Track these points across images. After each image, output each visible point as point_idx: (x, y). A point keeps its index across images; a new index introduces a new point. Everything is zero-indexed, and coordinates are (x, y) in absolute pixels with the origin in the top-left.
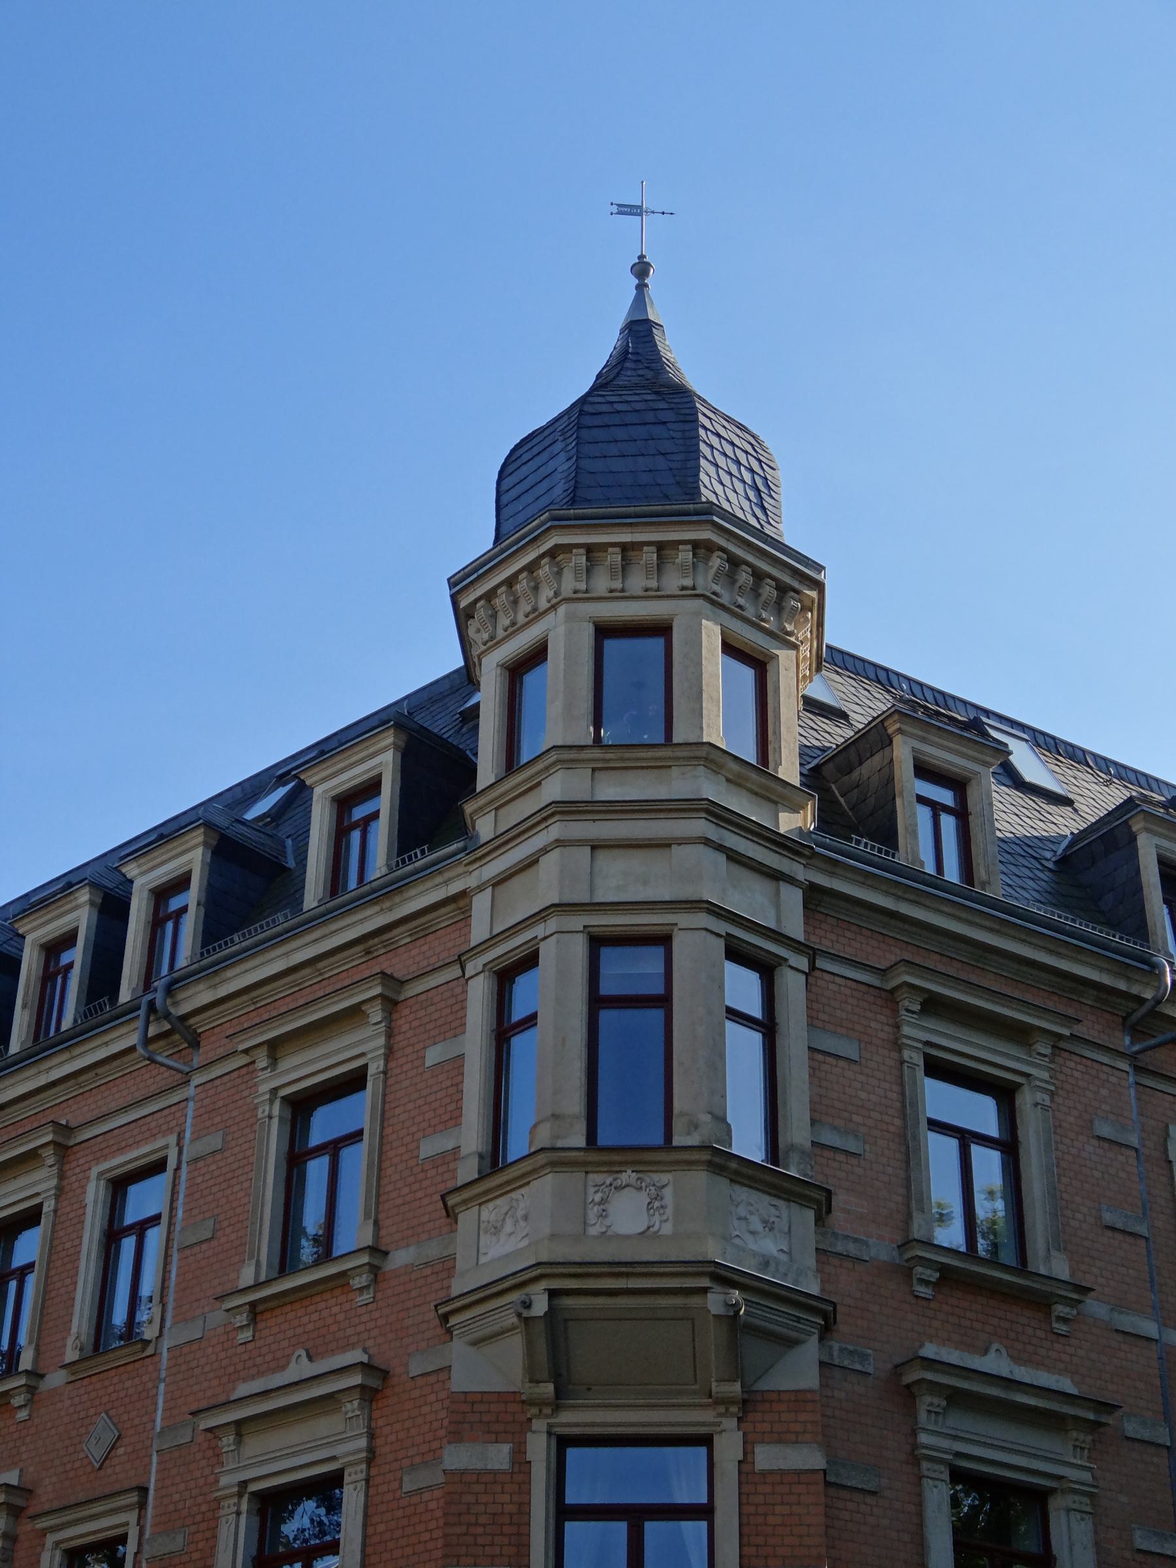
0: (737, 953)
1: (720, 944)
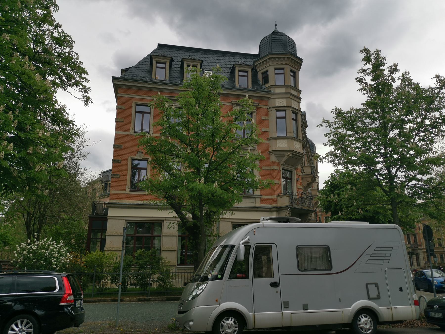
0: (293, 112)
1: (291, 111)
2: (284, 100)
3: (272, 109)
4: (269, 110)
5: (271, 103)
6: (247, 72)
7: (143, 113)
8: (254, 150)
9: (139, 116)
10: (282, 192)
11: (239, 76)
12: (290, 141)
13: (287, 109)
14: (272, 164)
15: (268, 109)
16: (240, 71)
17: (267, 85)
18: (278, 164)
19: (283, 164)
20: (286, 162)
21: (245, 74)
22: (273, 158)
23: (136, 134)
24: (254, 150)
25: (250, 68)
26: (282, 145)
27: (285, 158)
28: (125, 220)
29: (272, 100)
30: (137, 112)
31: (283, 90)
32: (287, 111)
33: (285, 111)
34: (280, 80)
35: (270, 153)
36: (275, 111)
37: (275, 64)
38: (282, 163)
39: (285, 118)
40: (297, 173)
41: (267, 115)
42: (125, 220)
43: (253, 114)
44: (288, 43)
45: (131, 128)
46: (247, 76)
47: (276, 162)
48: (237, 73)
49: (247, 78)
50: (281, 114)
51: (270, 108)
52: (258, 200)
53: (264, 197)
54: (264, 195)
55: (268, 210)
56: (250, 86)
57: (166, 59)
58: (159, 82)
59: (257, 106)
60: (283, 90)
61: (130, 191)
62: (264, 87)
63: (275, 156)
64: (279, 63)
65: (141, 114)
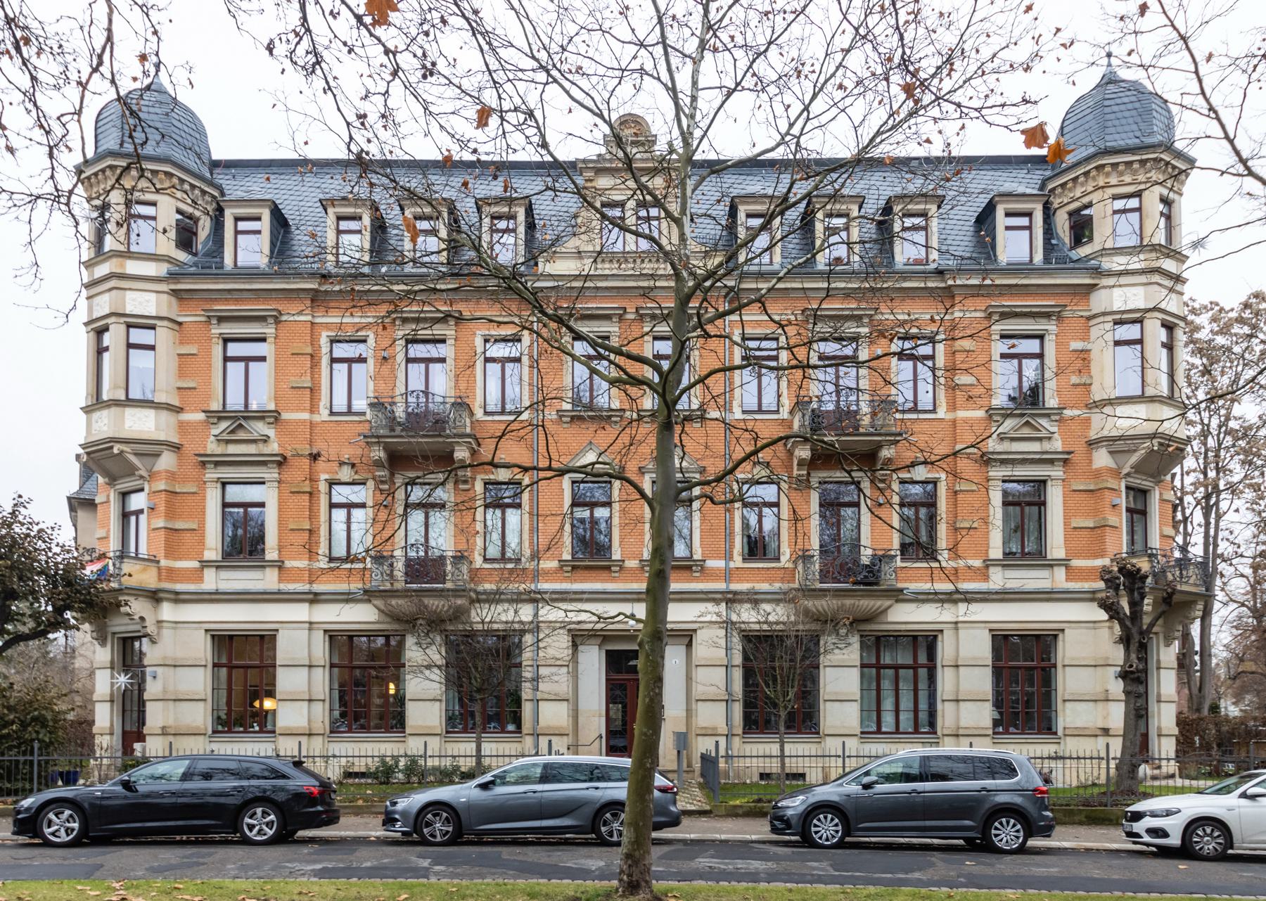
1: (1159, 323)
2: (1140, 291)
3: (1101, 319)
4: (1092, 322)
5: (1099, 301)
6: (1029, 214)
7: (247, 360)
8: (1050, 438)
9: (494, 369)
10: (1125, 550)
11: (1008, 228)
12: (114, 410)
13: (109, 321)
14: (1097, 474)
15: (1089, 318)
16: (1008, 215)
17: (1084, 251)
18: (1116, 473)
19: (1128, 475)
20: (1138, 469)
21: (1024, 221)
22: (1102, 459)
23: (490, 418)
24: (1050, 438)
25: (520, 205)
26: (1130, 420)
27: (1134, 458)
28: (325, 631)
29: (1103, 291)
30: (487, 360)
31: (1136, 263)
32: (1146, 322)
33: (1140, 321)
34: (1125, 231)
35: (1092, 444)
36: (123, 327)
37: (1114, 181)
38: (1126, 470)
39: (152, 348)
40: (1161, 494)
41: (1086, 338)
42: (207, 631)
43: (1047, 338)
44: (1155, 114)
45: (322, 404)
46: (1029, 228)
47: (1111, 469)
48: (1001, 220)
49: (1027, 232)
50: (1132, 332)
51: (1094, 317)
52: (1060, 573)
53: (1076, 563)
54: (710, 558)
55: (635, 596)
56: (1039, 257)
57: (1033, 202)
58: (1015, 269)
59: (621, 316)
60: (1136, 263)
61: (744, 560)
62: (1074, 255)
63: (1110, 453)
64: (1128, 179)
65: (346, 365)
